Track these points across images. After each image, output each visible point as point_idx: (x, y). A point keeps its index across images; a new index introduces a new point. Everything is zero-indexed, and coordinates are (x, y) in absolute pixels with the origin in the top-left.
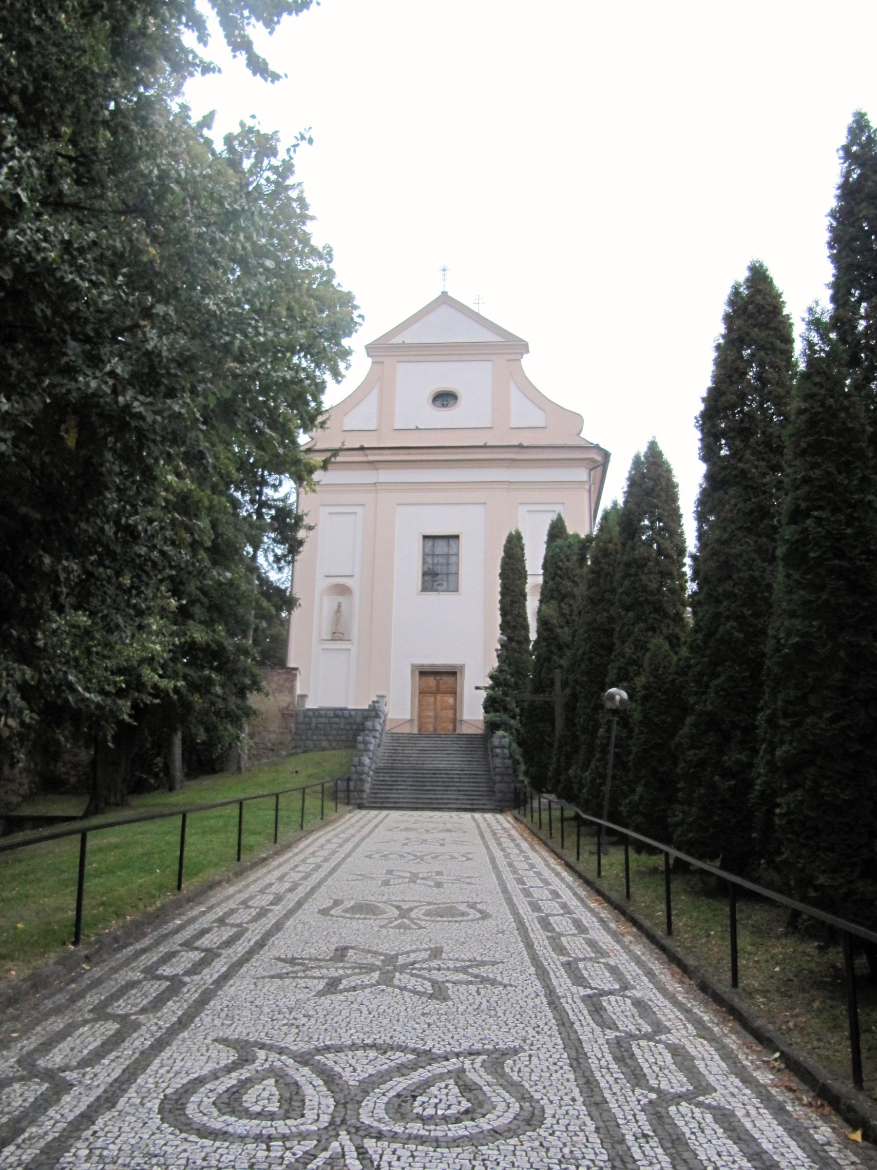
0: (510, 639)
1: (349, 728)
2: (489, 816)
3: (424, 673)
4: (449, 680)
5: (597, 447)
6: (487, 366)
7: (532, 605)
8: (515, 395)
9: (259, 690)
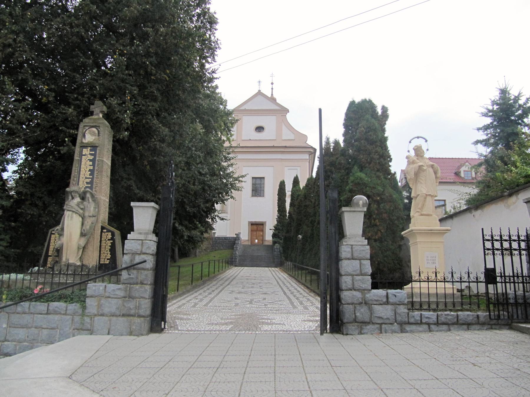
0: (280, 215)
1: (231, 243)
2: (273, 268)
3: (252, 224)
4: (262, 226)
5: (312, 147)
6: (275, 117)
7: (288, 200)
8: (284, 127)
9: (207, 233)
